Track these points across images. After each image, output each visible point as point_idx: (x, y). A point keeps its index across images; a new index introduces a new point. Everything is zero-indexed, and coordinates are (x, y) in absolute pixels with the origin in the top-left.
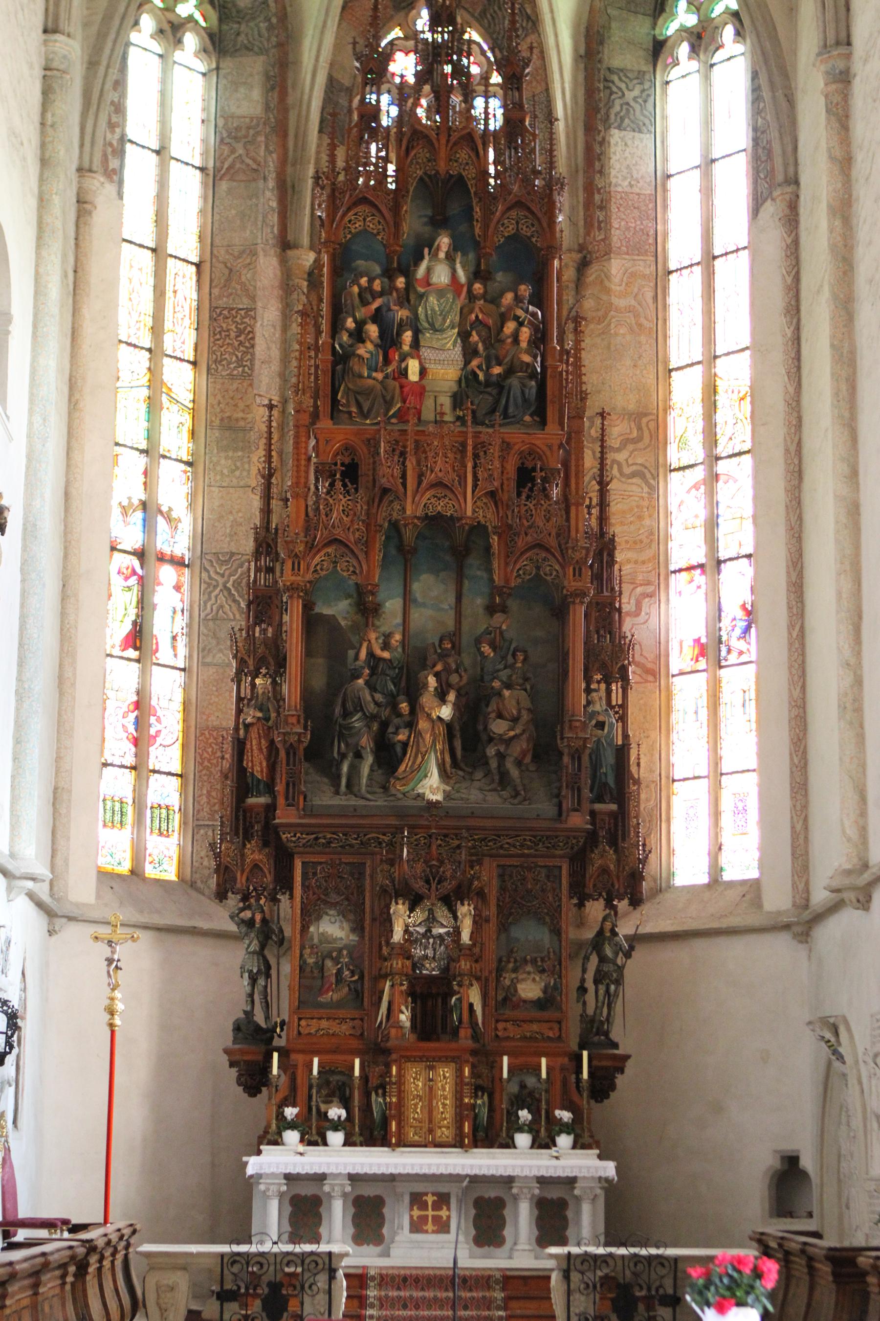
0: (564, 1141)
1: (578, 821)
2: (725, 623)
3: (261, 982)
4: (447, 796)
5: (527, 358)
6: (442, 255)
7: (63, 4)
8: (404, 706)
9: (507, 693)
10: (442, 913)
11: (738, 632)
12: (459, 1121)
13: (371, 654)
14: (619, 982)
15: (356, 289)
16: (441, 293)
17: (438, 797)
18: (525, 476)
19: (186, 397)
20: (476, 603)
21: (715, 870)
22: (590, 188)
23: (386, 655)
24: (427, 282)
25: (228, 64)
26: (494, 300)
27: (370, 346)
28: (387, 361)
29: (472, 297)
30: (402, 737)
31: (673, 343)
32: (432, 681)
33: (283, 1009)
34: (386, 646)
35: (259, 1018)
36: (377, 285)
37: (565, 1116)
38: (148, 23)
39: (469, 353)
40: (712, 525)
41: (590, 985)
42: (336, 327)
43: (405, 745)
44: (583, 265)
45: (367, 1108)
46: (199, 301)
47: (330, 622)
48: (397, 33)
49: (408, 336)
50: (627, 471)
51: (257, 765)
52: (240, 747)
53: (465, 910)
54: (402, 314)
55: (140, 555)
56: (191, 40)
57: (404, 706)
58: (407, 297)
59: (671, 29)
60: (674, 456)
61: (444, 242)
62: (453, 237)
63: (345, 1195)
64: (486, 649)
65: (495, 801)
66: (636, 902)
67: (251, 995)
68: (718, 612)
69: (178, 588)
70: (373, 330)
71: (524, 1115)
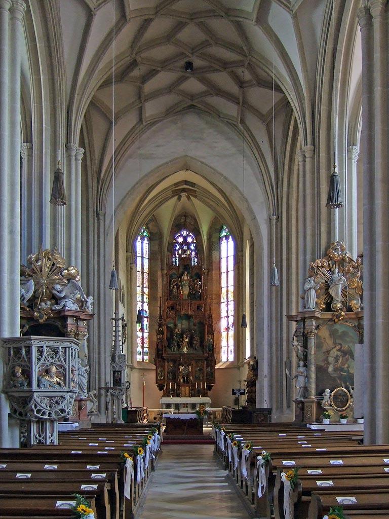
1: (206, 355)
2: (229, 325)
16: (186, 281)
18: (198, 308)
19: (147, 293)
20: (192, 324)
25: (152, 242)
29: (190, 281)
39: (190, 289)
40: (227, 311)
45: (177, 392)
47: (170, 327)
48: (179, 234)
51: (160, 347)
52: (157, 345)
54: (180, 284)
56: (146, 239)
58: (181, 281)
60: (222, 300)
61: (186, 273)
65: (194, 352)
68: (228, 324)
70: (176, 287)
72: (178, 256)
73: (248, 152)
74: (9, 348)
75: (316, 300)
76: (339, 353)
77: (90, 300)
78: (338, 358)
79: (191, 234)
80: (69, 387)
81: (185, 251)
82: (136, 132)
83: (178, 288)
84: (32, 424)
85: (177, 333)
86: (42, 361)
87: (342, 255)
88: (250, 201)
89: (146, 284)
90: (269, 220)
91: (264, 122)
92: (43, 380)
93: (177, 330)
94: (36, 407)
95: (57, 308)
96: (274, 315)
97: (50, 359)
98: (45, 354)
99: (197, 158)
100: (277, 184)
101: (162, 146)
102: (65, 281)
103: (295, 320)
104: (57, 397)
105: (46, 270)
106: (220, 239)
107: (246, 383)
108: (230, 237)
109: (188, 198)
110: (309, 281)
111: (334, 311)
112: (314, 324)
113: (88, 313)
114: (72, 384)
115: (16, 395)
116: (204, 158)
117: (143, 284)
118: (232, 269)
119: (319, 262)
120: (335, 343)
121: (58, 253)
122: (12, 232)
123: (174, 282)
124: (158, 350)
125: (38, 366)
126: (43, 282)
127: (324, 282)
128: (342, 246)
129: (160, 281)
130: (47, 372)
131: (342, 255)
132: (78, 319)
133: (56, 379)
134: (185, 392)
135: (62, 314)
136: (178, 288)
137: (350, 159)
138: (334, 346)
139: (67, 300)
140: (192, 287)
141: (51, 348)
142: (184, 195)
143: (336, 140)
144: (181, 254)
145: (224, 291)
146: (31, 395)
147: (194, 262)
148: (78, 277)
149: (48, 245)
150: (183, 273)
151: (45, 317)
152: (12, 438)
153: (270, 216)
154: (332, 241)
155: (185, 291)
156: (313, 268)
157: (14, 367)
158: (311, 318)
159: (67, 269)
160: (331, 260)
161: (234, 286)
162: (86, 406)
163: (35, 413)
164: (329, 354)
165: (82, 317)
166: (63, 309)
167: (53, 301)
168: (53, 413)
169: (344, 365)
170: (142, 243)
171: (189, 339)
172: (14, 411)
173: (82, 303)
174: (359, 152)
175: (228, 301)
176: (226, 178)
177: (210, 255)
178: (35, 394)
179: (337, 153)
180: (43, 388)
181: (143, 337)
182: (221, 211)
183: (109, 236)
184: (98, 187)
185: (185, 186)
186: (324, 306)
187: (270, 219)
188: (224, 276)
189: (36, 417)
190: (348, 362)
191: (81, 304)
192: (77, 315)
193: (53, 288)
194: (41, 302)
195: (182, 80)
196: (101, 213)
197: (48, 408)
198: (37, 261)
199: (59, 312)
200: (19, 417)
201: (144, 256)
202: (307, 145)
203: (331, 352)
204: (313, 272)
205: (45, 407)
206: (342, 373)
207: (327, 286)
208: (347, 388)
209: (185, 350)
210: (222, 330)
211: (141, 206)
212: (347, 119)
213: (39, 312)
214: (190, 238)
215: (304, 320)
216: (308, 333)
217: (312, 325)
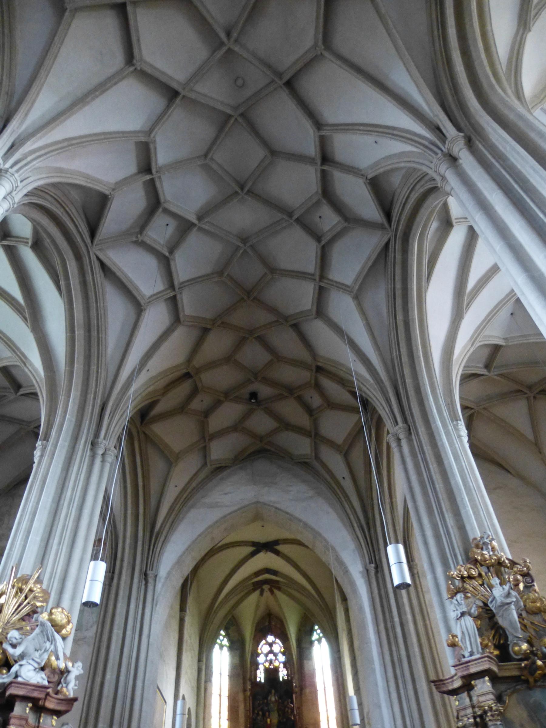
31: (470, 536)
36: (261, 702)
39: (279, 715)
42: (253, 712)
49: (267, 713)
54: (266, 708)
56: (225, 649)
58: (268, 704)
61: (273, 691)
70: (260, 713)
83: (264, 715)
87: (496, 555)
88: (338, 549)
90: (365, 572)
100: (368, 524)
101: (230, 493)
109: (272, 592)
113: (65, 695)
119: (462, 569)
131: (496, 555)
136: (264, 715)
139: (23, 662)
142: (266, 587)
143: (435, 411)
147: (283, 674)
148: (69, 627)
150: (269, 692)
182: (309, 603)
183: (158, 606)
185: (267, 576)
186: (496, 652)
187: (367, 570)
192: (35, 694)
195: (246, 416)
196: (151, 573)
202: (397, 424)
212: (440, 391)
214: (277, 645)
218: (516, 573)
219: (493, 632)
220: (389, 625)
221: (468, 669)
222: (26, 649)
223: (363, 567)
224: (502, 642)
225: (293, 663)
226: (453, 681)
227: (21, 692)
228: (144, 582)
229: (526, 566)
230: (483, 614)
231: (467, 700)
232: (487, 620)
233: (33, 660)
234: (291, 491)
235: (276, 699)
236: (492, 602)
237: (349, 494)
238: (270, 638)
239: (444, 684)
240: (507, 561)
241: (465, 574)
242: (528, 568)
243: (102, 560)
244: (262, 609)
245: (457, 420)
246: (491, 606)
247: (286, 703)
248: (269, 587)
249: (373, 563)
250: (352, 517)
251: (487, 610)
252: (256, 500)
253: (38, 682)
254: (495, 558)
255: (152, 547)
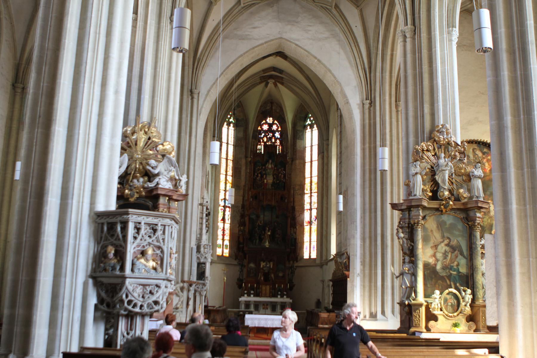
0: (285, 297)
3: (241, 272)
4: (269, 246)
5: (283, 180)
6: (270, 163)
7: (181, 1)
8: (263, 232)
9: (278, 231)
10: (268, 263)
11: (314, 220)
12: (270, 294)
13: (258, 224)
14: (294, 273)
15: (257, 169)
16: (270, 169)
17: (267, 246)
21: (310, 256)
22: (294, 149)
23: (261, 224)
24: (268, 167)
26: (278, 170)
27: (259, 178)
28: (262, 180)
29: (274, 170)
30: (263, 237)
32: (267, 229)
33: (245, 276)
34: (261, 223)
35: (241, 278)
36: (260, 168)
37: (285, 293)
38: (225, 123)
39: (274, 178)
40: (311, 203)
41: (290, 274)
43: (263, 238)
44: (292, 161)
46: (233, 166)
48: (264, 122)
49: (265, 176)
50: (298, 194)
51: (241, 240)
52: (239, 238)
53: (271, 263)
54: (264, 172)
55: (223, 206)
56: (232, 125)
57: (263, 232)
58: (265, 170)
59: (307, 124)
60: (306, 192)
61: (270, 161)
62: (272, 161)
63: (253, 304)
64: (275, 224)
66: (297, 261)
67: (240, 275)
69: (229, 211)
70: (259, 175)
71: (279, 293)
72: (263, 144)
73: (342, 36)
74: (103, 224)
75: (422, 187)
76: (447, 248)
77: (184, 179)
78: (447, 254)
79: (276, 122)
80: (166, 274)
81: (270, 139)
82: (234, 13)
83: (262, 177)
84: (120, 318)
85: (259, 225)
86: (138, 241)
87: (447, 139)
88: (343, 84)
89: (230, 172)
91: (358, 7)
92: (138, 263)
93: (259, 222)
94: (127, 296)
95: (150, 186)
96: (367, 206)
97: (148, 238)
98: (142, 232)
99: (292, 40)
100: (370, 68)
101: (259, 27)
102: (159, 156)
103: (400, 208)
104: (152, 285)
105: (141, 144)
106: (305, 127)
107: (331, 283)
108: (315, 126)
109: (276, 85)
110: (415, 165)
111: (442, 200)
112: (421, 214)
114: (169, 271)
115: (105, 280)
116: (298, 40)
117: (226, 171)
118: (317, 159)
119: (424, 145)
120: (443, 237)
121: (155, 127)
122: (117, 92)
123: (259, 170)
124: (239, 243)
125: (135, 245)
126: (137, 156)
127: (430, 167)
128: (447, 130)
129: (243, 168)
130: (143, 253)
131: (447, 139)
132: (170, 199)
133: (152, 264)
134: (266, 292)
135: (155, 193)
136: (262, 177)
137: (451, 40)
138: (442, 240)
140: (276, 176)
141: (149, 224)
144: (267, 142)
145: (307, 181)
146: (122, 282)
147: (279, 150)
149: (145, 117)
150: (267, 161)
151: (136, 196)
152: (96, 335)
153: (362, 101)
154: (436, 124)
155: (269, 180)
156: (417, 152)
157: (106, 246)
158: (418, 206)
159: (162, 144)
160: (437, 143)
161: (318, 176)
162: (172, 301)
163: (126, 304)
164: (436, 249)
165: (174, 197)
166: (156, 188)
167: (146, 178)
168: (145, 306)
169: (453, 263)
170: (228, 128)
171: (271, 232)
172: (101, 300)
173: (176, 182)
174: (458, 34)
175: (311, 193)
176: (319, 60)
177: (294, 144)
178: (128, 281)
179: (438, 34)
180: (136, 274)
181: (224, 228)
182: (307, 99)
184: (194, 65)
185: (273, 73)
186: (430, 194)
187: (363, 104)
188: (308, 166)
189: (126, 309)
190: (457, 260)
191: (174, 182)
192: (170, 194)
193: (148, 164)
194: (133, 178)
196: (196, 91)
197: (141, 299)
198: (133, 133)
199: (151, 190)
200: (106, 309)
201: (229, 143)
202: (407, 25)
203: (439, 247)
204: (418, 156)
205: (137, 297)
206: (452, 272)
207: (433, 172)
208: (457, 288)
209: (267, 244)
210: (305, 224)
211: (229, 91)
213: (131, 190)
215: (409, 209)
216: (415, 223)
217: (419, 215)
218: (457, 151)
219: (432, 183)
220: (372, 145)
221: (411, 203)
222: (160, 170)
223: (360, 101)
224: (435, 189)
225: (288, 141)
226: (402, 205)
227: (163, 193)
228: (190, 97)
229: (464, 147)
230: (429, 172)
231: (408, 215)
232: (431, 176)
233: (165, 176)
234: (310, 31)
235: (272, 166)
236: (436, 166)
237: (359, 41)
238: (270, 120)
239: (397, 206)
240: (453, 143)
241: (425, 148)
242: (465, 149)
243: (217, 141)
244: (265, 95)
245: (453, 27)
246: (435, 169)
247: (280, 170)
248: (274, 81)
249: (368, 100)
250: (358, 60)
251: (432, 171)
252: (279, 36)
253: (169, 188)
254: (447, 140)
255: (195, 70)
